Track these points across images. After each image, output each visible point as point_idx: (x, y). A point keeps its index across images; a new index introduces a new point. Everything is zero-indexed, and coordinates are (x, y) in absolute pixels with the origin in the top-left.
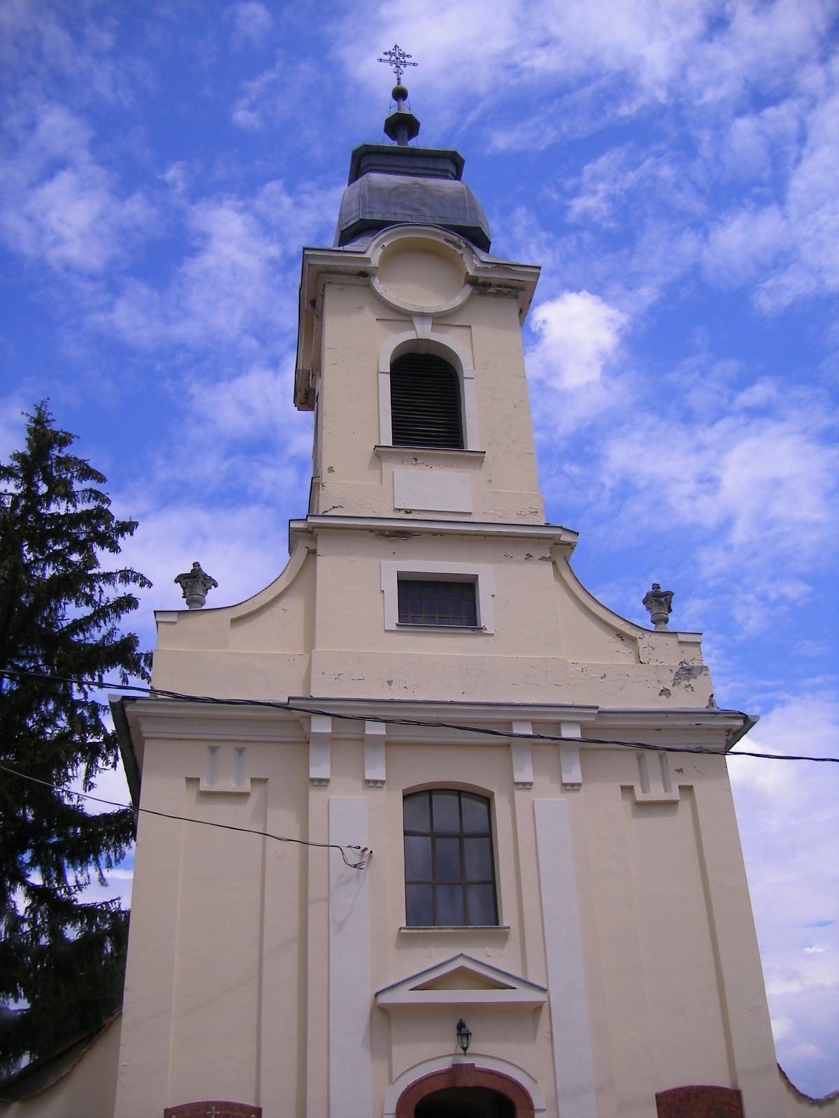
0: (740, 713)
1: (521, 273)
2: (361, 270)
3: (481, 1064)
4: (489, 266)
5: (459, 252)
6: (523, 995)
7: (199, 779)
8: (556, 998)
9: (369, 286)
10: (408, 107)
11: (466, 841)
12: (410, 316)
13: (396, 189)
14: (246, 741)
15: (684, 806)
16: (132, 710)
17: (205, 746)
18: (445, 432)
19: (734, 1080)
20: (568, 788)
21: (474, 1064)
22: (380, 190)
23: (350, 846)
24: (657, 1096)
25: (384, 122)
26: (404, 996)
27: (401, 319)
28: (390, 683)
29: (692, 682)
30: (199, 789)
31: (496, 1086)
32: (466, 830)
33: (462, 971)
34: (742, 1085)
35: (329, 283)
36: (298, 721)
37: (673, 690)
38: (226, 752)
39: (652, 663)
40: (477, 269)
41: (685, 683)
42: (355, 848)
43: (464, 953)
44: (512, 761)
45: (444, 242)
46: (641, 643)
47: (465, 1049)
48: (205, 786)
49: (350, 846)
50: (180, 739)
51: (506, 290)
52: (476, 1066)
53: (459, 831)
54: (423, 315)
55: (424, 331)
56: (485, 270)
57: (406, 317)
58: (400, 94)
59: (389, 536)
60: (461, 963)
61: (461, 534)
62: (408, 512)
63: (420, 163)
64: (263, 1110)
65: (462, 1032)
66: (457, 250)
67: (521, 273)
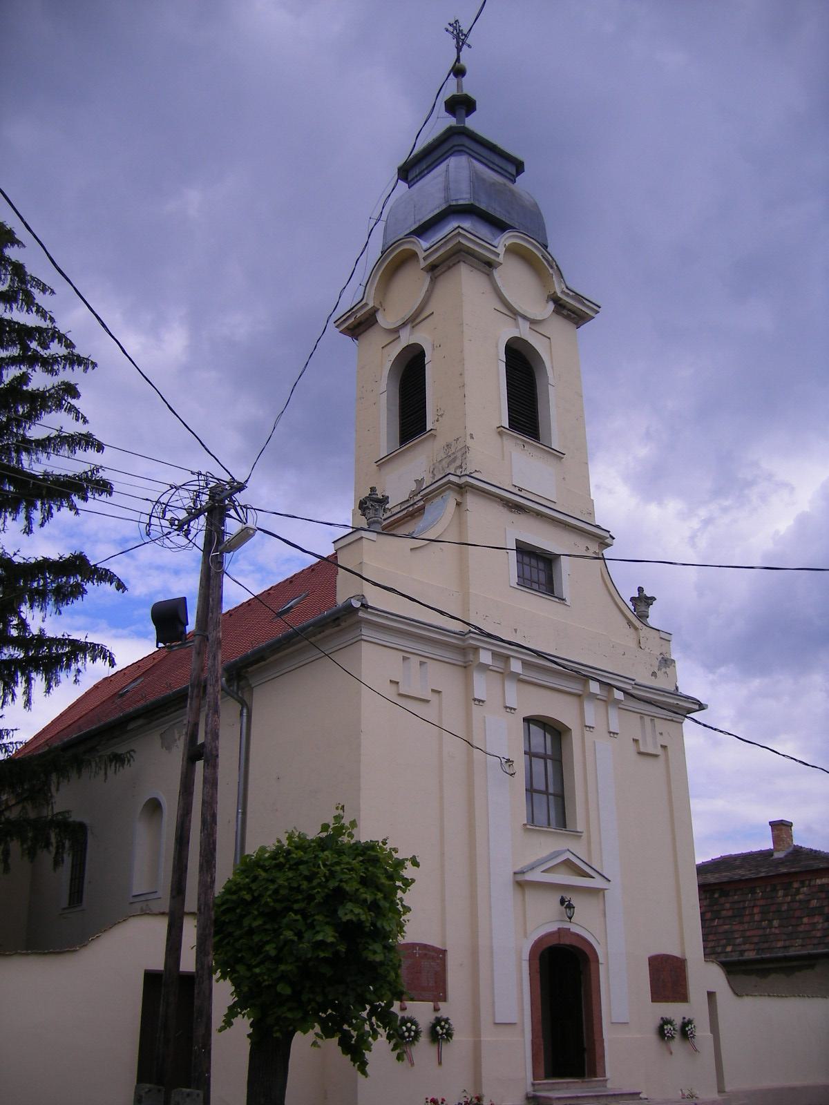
0: (699, 701)
1: (588, 307)
2: (490, 260)
3: (575, 929)
4: (571, 293)
5: (551, 271)
6: (597, 883)
9: (490, 276)
10: (470, 87)
12: (515, 314)
13: (494, 184)
15: (662, 758)
16: (362, 616)
18: (524, 422)
19: (684, 953)
22: (483, 180)
25: (452, 95)
26: (536, 876)
27: (507, 313)
28: (516, 630)
29: (668, 670)
34: (688, 957)
35: (464, 261)
36: (464, 649)
37: (659, 673)
39: (647, 650)
40: (563, 292)
41: (664, 670)
44: (583, 709)
45: (541, 257)
46: (642, 634)
47: (570, 918)
51: (573, 315)
52: (571, 930)
54: (525, 317)
55: (524, 331)
56: (567, 295)
57: (514, 313)
58: (459, 72)
59: (511, 507)
60: (568, 855)
61: (552, 520)
62: (520, 490)
63: (496, 159)
64: (448, 953)
65: (566, 905)
66: (549, 269)
67: (588, 307)
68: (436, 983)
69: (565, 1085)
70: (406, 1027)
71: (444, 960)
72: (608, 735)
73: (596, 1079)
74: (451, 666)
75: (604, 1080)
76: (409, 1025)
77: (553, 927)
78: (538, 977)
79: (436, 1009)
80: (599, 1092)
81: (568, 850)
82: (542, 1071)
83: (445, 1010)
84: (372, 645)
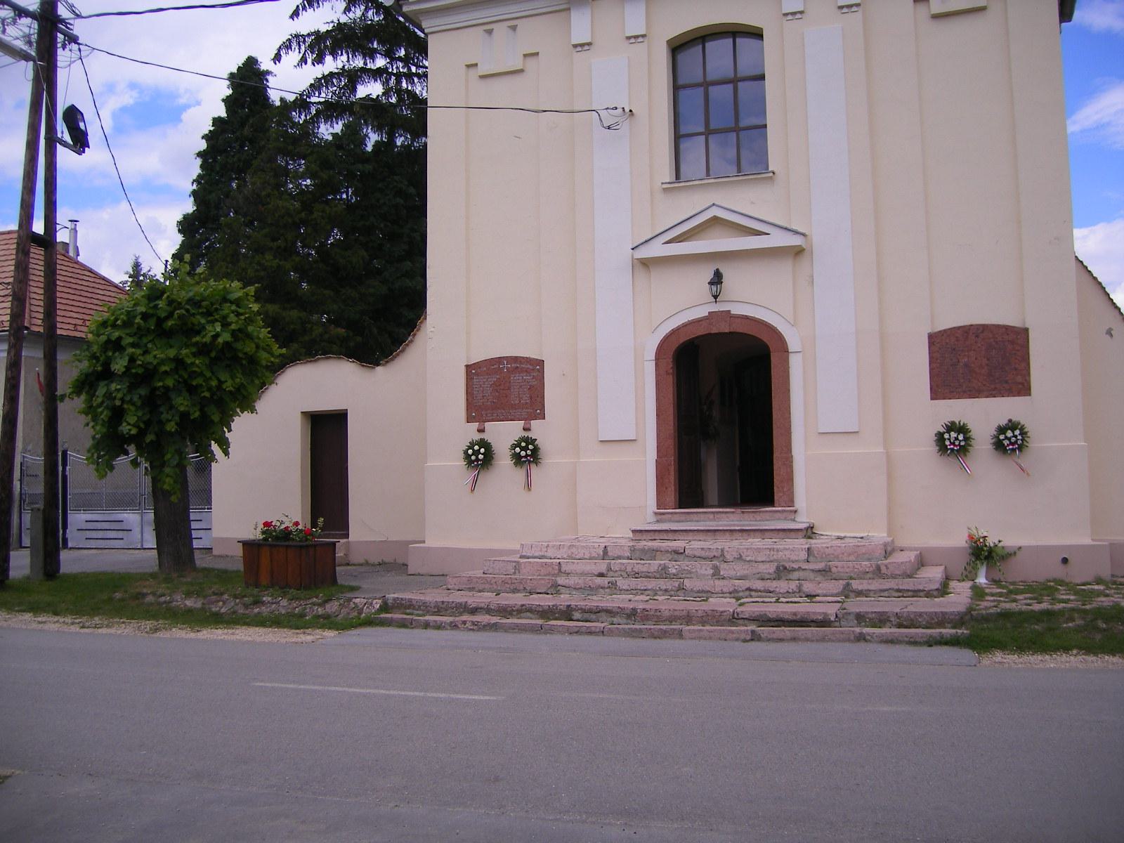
3: (737, 310)
7: (538, 53)
8: (818, 239)
11: (740, 84)
14: (517, 18)
16: (407, 10)
17: (480, 29)
20: (845, 10)
21: (729, 311)
23: (607, 108)
24: (933, 338)
26: (657, 250)
30: (930, 12)
31: (669, 363)
32: (709, 78)
33: (715, 221)
38: (501, 30)
42: (612, 109)
43: (717, 203)
48: (484, 69)
49: (607, 108)
50: (458, 29)
52: (732, 313)
53: (733, 76)
68: (531, 398)
69: (711, 516)
70: (472, 455)
71: (542, 371)
72: (839, 12)
73: (774, 509)
74: (557, 14)
75: (791, 511)
76: (482, 450)
77: (701, 312)
78: (670, 380)
79: (481, 431)
80: (744, 525)
81: (714, 204)
82: (671, 496)
83: (538, 430)
84: (466, 30)
